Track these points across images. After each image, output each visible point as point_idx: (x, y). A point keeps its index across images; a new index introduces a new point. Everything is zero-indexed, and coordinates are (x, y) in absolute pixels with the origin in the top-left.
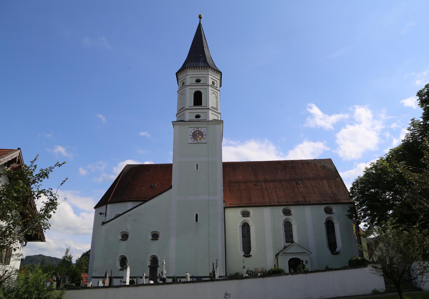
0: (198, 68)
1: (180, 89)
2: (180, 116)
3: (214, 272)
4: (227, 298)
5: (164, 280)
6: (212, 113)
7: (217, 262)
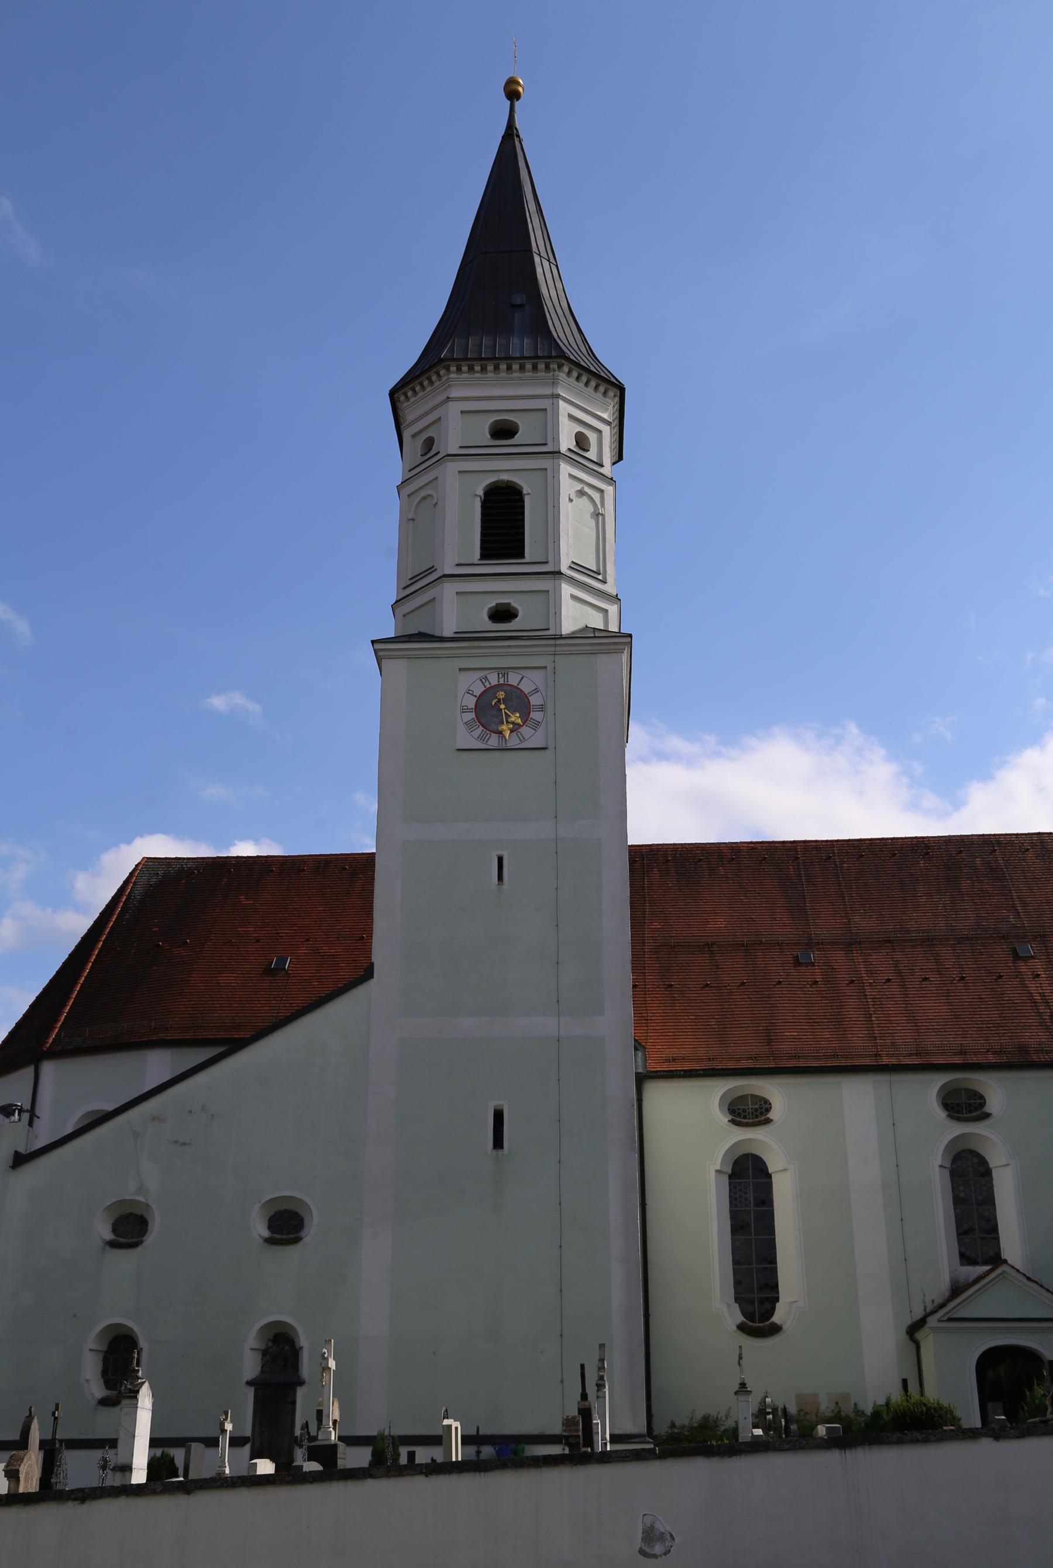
0: (503, 367)
2: (413, 611)
3: (586, 1414)
4: (655, 1556)
5: (326, 1454)
6: (573, 597)
7: (602, 1360)
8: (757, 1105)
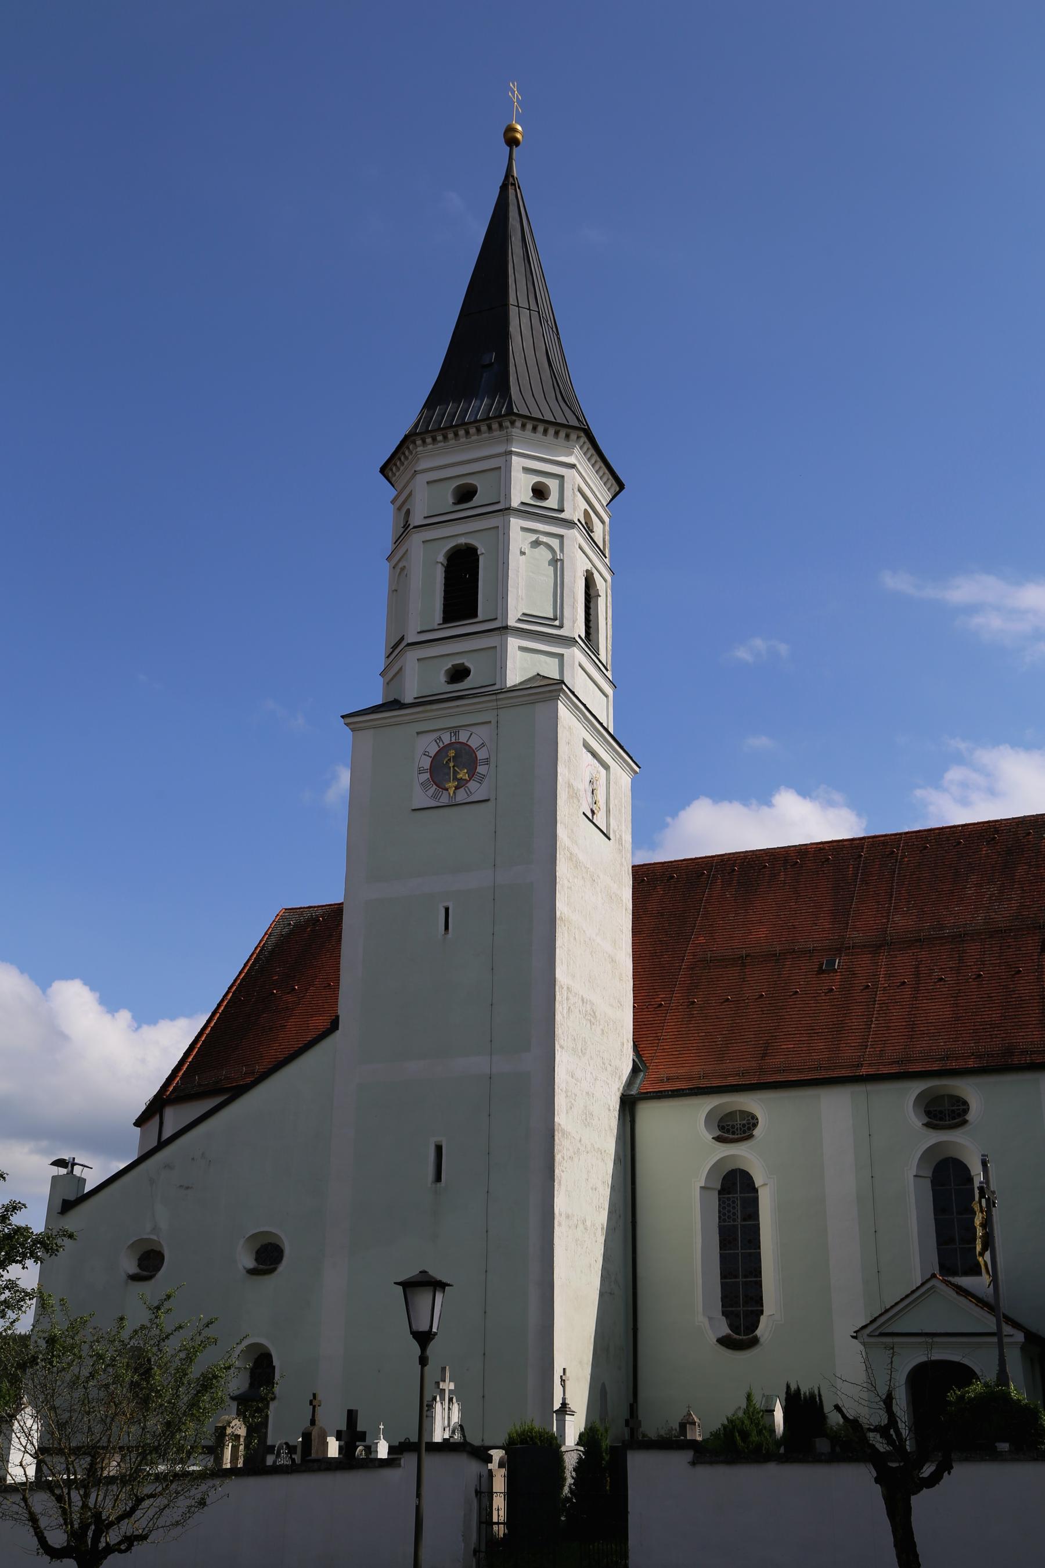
1: (397, 544)
8: (744, 1120)
